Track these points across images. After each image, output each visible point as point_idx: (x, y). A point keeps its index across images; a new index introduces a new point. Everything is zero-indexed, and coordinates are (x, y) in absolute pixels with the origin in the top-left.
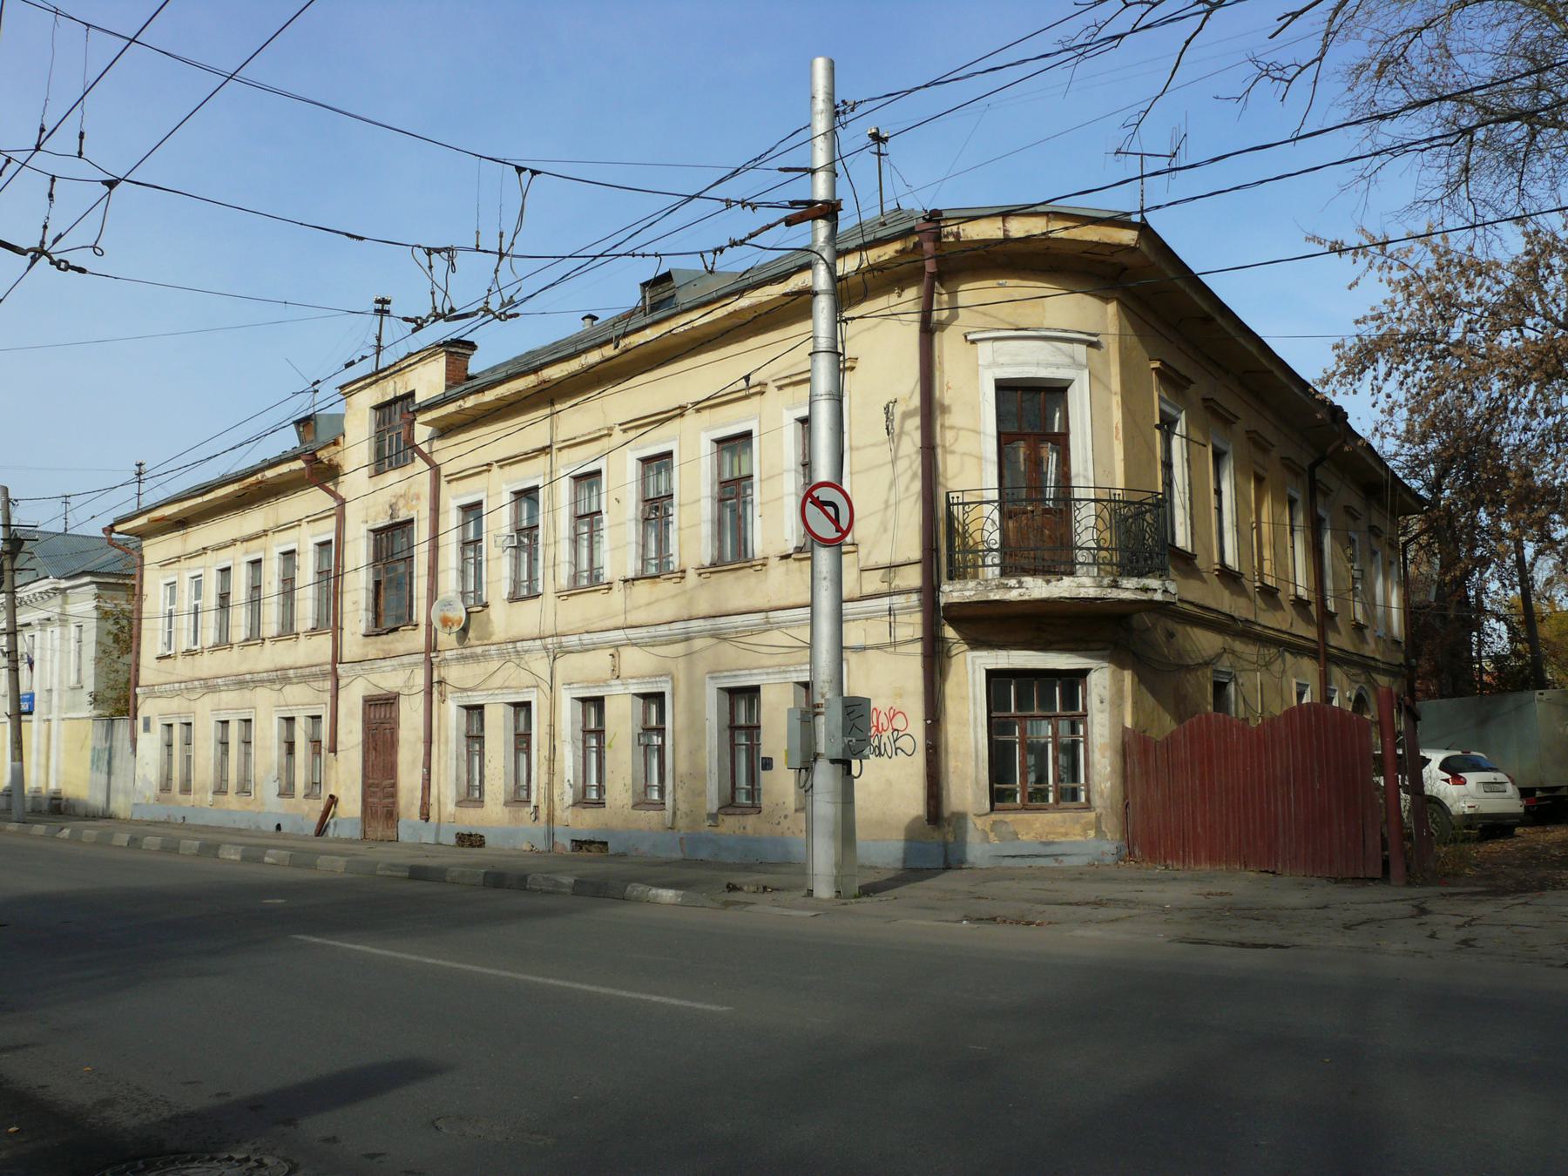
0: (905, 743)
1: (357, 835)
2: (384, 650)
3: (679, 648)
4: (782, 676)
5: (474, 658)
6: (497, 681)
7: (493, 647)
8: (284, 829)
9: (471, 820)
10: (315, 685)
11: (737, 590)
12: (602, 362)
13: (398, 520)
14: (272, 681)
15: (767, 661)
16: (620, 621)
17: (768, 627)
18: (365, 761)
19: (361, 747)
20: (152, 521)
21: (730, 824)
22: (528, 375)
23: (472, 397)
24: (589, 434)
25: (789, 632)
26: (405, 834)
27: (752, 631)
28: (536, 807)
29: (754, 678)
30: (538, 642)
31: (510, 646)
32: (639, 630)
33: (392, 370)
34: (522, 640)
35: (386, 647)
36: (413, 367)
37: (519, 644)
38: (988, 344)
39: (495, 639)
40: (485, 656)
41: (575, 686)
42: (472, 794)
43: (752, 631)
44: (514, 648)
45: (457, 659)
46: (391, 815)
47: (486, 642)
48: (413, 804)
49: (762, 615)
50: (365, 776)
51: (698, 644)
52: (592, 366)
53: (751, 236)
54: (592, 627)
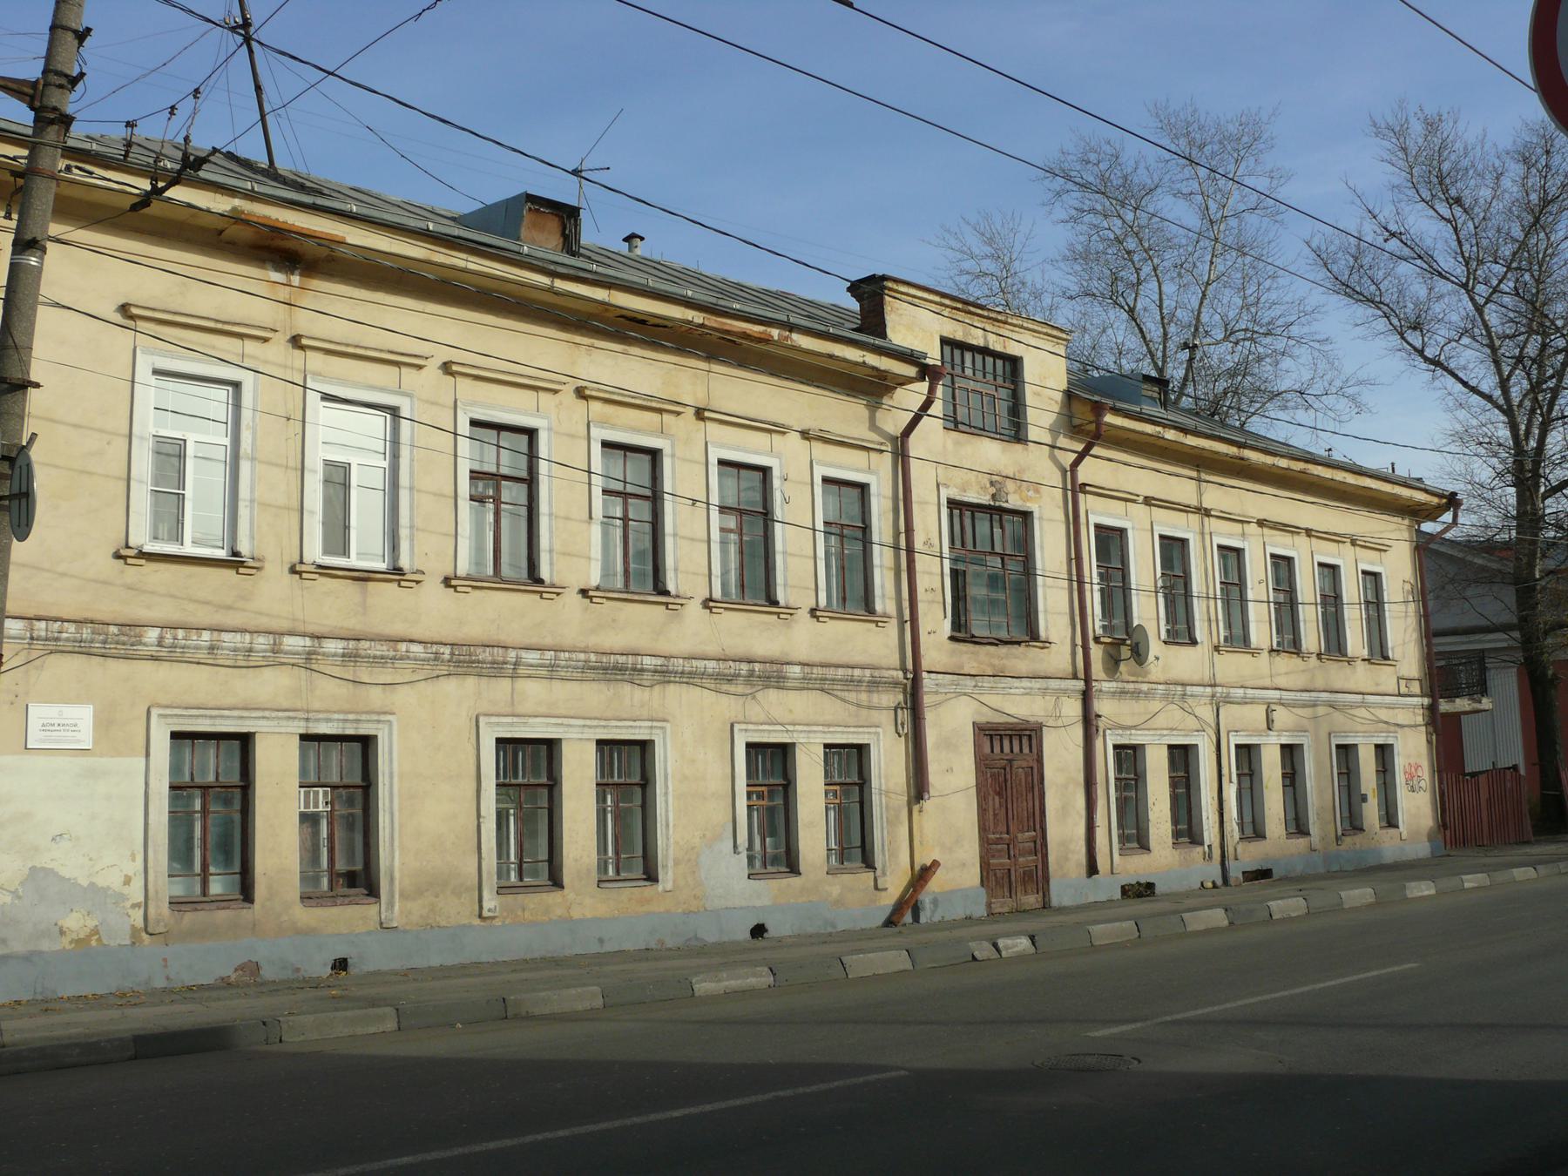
0: (1423, 784)
1: (981, 911)
2: (993, 666)
3: (1307, 712)
4: (606, 731)
5: (1136, 695)
6: (1160, 721)
7: (1160, 687)
8: (773, 932)
9: (1135, 867)
10: (852, 696)
11: (1337, 675)
12: (1286, 469)
13: (1005, 505)
14: (720, 677)
15: (1360, 728)
16: (1267, 682)
17: (1363, 705)
18: (982, 811)
19: (973, 791)
20: (236, 218)
21: (1348, 840)
22: (1232, 445)
23: (1172, 431)
24: (858, 439)
25: (982, 699)
26: (1060, 894)
27: (1353, 706)
28: (1209, 846)
29: (247, 722)
30: (1209, 690)
31: (1179, 688)
32: (1289, 693)
33: (986, 313)
34: (411, 641)
35: (996, 662)
36: (1022, 331)
37: (1188, 688)
38: (468, 381)
39: (1152, 677)
40: (1148, 695)
41: (1242, 733)
42: (1254, 829)
43: (1353, 706)
44: (1178, 690)
45: (1115, 693)
46: (1039, 878)
47: (1140, 679)
48: (1067, 859)
49: (1361, 696)
50: (983, 829)
51: (1321, 710)
52: (1371, 489)
53: (145, 76)
54: (1247, 684)
